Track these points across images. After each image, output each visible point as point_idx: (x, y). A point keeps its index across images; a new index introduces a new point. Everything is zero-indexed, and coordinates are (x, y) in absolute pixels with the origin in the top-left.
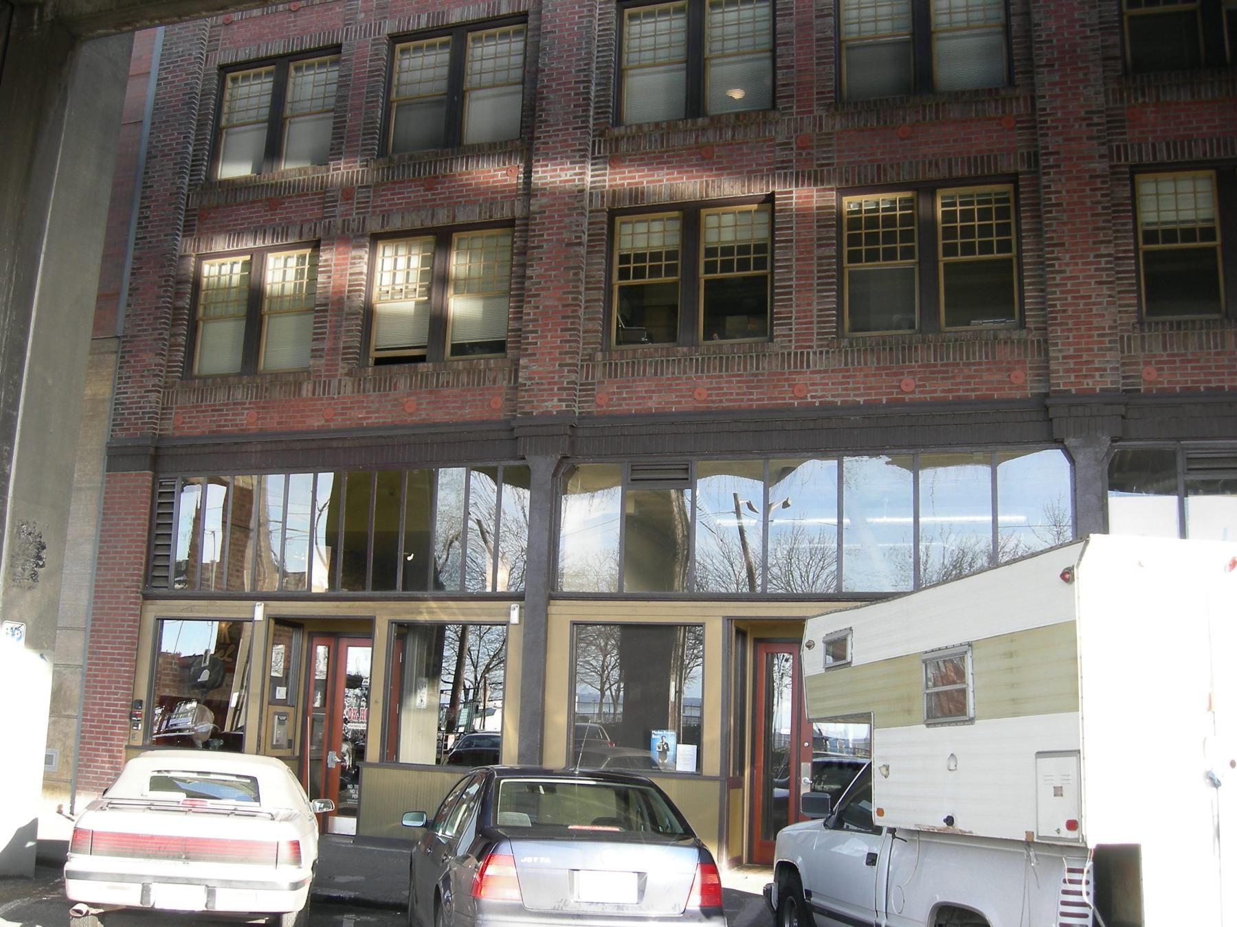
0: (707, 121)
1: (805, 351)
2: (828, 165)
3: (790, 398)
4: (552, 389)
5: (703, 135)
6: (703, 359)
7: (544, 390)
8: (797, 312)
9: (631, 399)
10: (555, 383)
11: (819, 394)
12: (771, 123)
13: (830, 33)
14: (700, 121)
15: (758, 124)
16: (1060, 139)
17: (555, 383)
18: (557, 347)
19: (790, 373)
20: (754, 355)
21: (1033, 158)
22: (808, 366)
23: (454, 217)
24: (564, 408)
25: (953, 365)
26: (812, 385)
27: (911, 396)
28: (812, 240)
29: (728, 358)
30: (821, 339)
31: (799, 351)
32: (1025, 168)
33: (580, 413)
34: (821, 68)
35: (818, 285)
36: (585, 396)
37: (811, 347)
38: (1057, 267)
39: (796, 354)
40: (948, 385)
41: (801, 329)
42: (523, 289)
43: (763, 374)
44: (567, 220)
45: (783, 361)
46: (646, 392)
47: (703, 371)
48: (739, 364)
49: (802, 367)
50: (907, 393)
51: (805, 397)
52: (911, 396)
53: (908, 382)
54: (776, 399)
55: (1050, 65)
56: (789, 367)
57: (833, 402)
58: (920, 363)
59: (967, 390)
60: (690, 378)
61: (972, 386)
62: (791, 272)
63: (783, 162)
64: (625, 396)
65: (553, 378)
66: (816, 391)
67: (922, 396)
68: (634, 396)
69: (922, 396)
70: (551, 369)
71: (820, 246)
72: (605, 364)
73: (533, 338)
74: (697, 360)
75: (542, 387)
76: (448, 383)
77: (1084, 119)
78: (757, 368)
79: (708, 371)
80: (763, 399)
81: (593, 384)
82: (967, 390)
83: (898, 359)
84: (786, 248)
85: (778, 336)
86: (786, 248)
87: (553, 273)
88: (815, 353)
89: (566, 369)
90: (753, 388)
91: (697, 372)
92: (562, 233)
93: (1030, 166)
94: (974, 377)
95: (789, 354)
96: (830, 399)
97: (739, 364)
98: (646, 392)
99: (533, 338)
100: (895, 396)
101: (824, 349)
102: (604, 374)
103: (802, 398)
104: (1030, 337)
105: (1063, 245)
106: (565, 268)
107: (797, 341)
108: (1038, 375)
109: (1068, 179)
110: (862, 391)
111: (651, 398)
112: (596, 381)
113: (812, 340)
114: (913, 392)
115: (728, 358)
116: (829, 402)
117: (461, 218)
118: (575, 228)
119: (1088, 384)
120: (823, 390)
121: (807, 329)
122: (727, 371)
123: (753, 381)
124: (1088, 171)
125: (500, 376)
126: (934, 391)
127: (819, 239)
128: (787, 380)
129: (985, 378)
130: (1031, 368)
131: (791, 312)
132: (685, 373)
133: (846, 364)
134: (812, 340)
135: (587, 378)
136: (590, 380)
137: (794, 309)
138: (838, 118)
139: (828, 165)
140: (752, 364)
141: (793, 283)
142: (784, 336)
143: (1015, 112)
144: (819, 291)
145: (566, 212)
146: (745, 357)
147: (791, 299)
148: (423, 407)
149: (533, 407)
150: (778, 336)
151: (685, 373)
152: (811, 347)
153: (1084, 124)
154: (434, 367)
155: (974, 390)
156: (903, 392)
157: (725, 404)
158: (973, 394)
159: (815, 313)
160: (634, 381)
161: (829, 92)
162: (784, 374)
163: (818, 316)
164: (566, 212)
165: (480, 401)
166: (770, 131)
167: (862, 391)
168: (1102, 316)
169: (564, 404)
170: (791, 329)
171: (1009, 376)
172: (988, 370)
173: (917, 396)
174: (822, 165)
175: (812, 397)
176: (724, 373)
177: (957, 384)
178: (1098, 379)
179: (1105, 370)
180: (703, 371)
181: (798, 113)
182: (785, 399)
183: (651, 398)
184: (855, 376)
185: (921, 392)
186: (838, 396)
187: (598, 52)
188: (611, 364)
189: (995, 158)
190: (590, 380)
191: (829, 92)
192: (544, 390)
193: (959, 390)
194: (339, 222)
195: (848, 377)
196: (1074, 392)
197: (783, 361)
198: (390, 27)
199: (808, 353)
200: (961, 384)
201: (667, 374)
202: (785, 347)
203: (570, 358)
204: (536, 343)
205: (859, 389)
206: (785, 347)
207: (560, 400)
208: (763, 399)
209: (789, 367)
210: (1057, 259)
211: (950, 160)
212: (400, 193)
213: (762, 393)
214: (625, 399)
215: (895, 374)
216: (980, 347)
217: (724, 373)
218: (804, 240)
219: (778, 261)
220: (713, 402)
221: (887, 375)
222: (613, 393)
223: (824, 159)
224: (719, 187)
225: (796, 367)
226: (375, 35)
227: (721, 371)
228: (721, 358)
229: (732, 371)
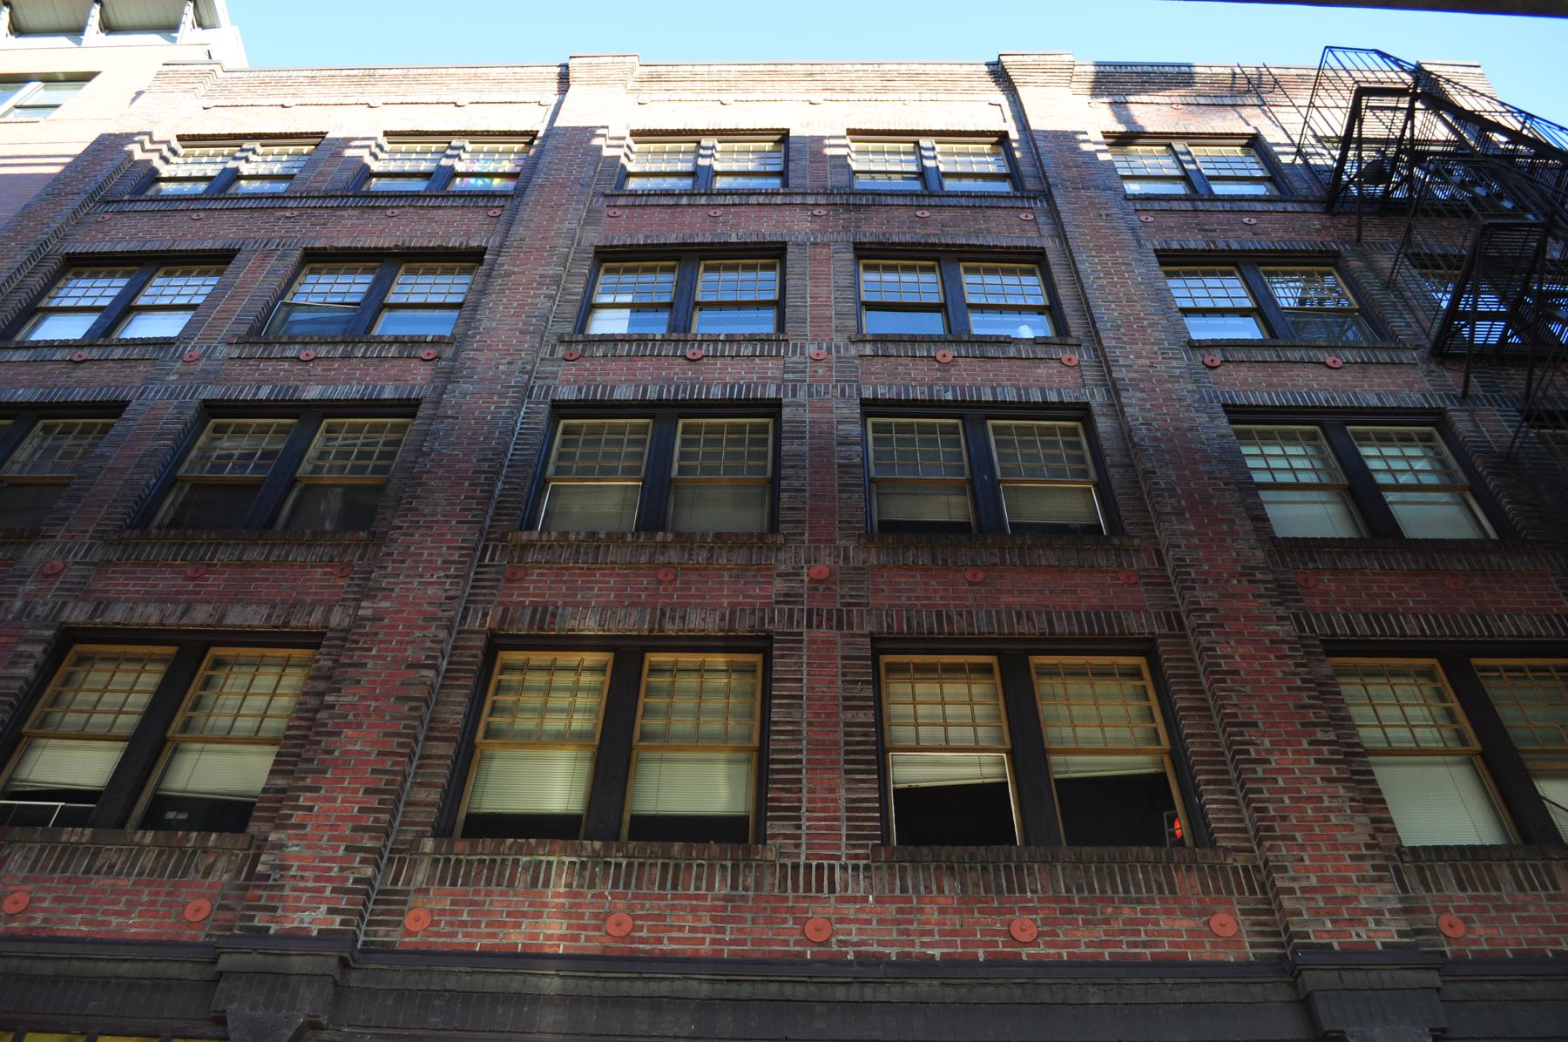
0: (670, 537)
1: (826, 863)
2: (859, 604)
3: (797, 943)
4: (320, 890)
5: (663, 554)
6: (630, 865)
7: (306, 890)
8: (810, 801)
9: (477, 924)
10: (330, 880)
11: (854, 938)
12: (770, 549)
13: (857, 460)
14: (660, 536)
15: (751, 549)
16: (1214, 594)
17: (330, 880)
18: (350, 818)
19: (797, 899)
20: (729, 863)
21: (1174, 621)
22: (832, 889)
23: (223, 617)
24: (337, 926)
25: (1101, 900)
26: (842, 921)
27: (1032, 951)
28: (835, 698)
29: (677, 866)
30: (854, 846)
31: (814, 863)
32: (1165, 630)
33: (365, 943)
34: (845, 496)
35: (846, 762)
36: (383, 913)
37: (838, 858)
38: (1253, 755)
39: (808, 867)
40: (1099, 933)
41: (816, 828)
42: (313, 720)
43: (743, 898)
44: (418, 634)
45: (784, 877)
46: (509, 914)
47: (627, 886)
48: (699, 878)
49: (820, 889)
50: (1026, 944)
51: (827, 943)
52: (1032, 951)
53: (1025, 925)
54: (769, 942)
55: (1179, 513)
56: (795, 888)
57: (883, 954)
58: (1040, 894)
59: (1135, 945)
60: (601, 896)
61: (1143, 937)
62: (800, 741)
63: (787, 595)
64: (465, 917)
65: (330, 869)
66: (849, 933)
67: (1052, 951)
68: (484, 920)
69: (1052, 951)
70: (330, 853)
71: (846, 708)
72: (437, 861)
73: (306, 799)
74: (618, 865)
75: (302, 884)
76: (111, 867)
77: (1242, 575)
78: (734, 887)
79: (638, 886)
80: (744, 942)
81: (407, 893)
82: (1135, 945)
83: (999, 886)
84: (790, 706)
85: (774, 836)
86: (790, 706)
87: (373, 704)
88: (844, 868)
89: (359, 856)
90: (724, 920)
91: (615, 885)
92: (406, 650)
93: (1171, 628)
94: (1144, 922)
95: (796, 867)
96: (875, 948)
97: (699, 878)
98: (509, 914)
99: (306, 799)
100: (1001, 949)
101: (862, 863)
102: (430, 879)
103: (820, 944)
104: (1230, 860)
105: (1255, 725)
106: (397, 698)
107: (809, 846)
108: (1259, 924)
109: (1239, 642)
110: (937, 937)
111: (518, 925)
112: (412, 887)
113: (838, 847)
114: (1033, 944)
115: (677, 866)
116: (874, 954)
117: (238, 617)
118: (429, 644)
119: (1359, 935)
120: (860, 931)
121: (827, 828)
122: (674, 887)
123: (725, 909)
124: (1267, 634)
125: (220, 866)
126: (1076, 944)
127: (846, 699)
128: (791, 910)
129: (1163, 926)
130: (1243, 912)
131: (800, 800)
132: (592, 885)
133: (904, 889)
134: (838, 847)
135: (395, 881)
136: (400, 886)
137: (805, 795)
138: (874, 551)
139: (859, 604)
140: (724, 880)
141: (803, 757)
142: (786, 836)
143: (1136, 566)
144: (847, 772)
145: (420, 622)
146: (711, 866)
147: (800, 781)
148: (45, 905)
149: (273, 920)
150: (774, 836)
151: (592, 885)
152: (838, 858)
153: (1244, 579)
154: (93, 836)
155: (1145, 945)
156: (1015, 942)
157: (667, 946)
158: (1147, 951)
159: (843, 804)
160: (488, 894)
161: (857, 522)
162: (786, 899)
163: (847, 753)
164: (420, 622)
165: (164, 904)
166: (767, 558)
167: (937, 937)
168: (1350, 828)
169: (338, 919)
170: (799, 827)
171: (1207, 923)
172: (1168, 912)
173: (1042, 950)
174: (850, 604)
175: (841, 943)
176: (669, 892)
177: (1113, 933)
178: (1372, 926)
179: (1380, 912)
180: (627, 886)
181: (849, 857)
182: (786, 943)
183: (518, 925)
184: (921, 910)
185: (1049, 945)
186: (892, 943)
187: (515, 449)
188: (448, 860)
189: (1118, 617)
190: (400, 886)
191: (857, 522)
192: (306, 890)
193: (1121, 942)
194: (18, 604)
195: (911, 911)
196: (1336, 946)
197: (784, 877)
198: (212, 392)
199: (832, 868)
200: (1122, 932)
201: (557, 885)
202: (788, 855)
203: (371, 838)
204: (310, 809)
205: (930, 933)
206: (788, 855)
207: (331, 911)
208: (744, 942)
209: (795, 888)
210: (1251, 743)
211: (1049, 614)
212: (142, 579)
213: (741, 931)
214: (464, 924)
215: (998, 911)
216: (1145, 872)
217: (669, 892)
218: (820, 699)
219: (776, 723)
220: (642, 941)
221: (981, 911)
222: (442, 912)
223: (851, 596)
224: (683, 618)
225: (808, 888)
226: (184, 398)
227: (662, 886)
228: (665, 866)
229: (686, 888)
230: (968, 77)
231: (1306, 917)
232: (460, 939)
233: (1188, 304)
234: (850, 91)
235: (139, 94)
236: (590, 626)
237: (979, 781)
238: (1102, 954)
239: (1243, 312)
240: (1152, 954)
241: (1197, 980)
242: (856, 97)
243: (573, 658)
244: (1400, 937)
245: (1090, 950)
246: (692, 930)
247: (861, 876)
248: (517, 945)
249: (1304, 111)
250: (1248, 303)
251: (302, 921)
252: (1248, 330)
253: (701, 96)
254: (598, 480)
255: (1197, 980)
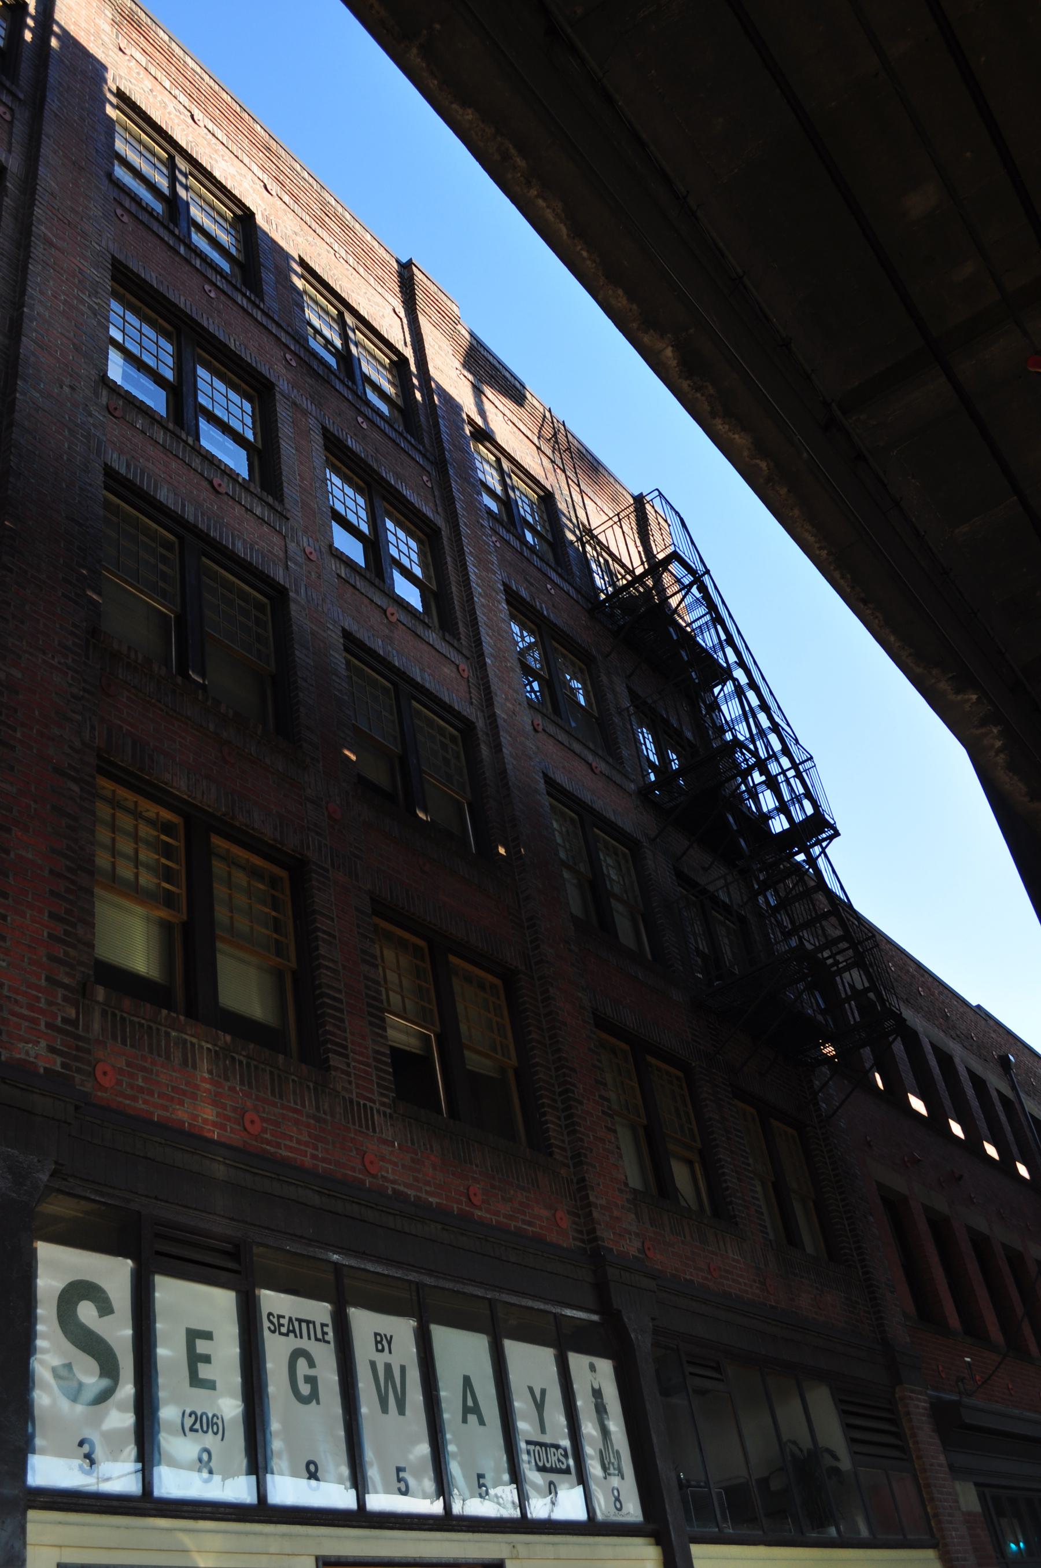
37: (374, 1102)
78: (318, 1109)
158: (530, 1229)
230: (383, 264)
231: (603, 1227)
232: (140, 1105)
233: (339, 507)
234: (296, 200)
235: (120, 49)
236: (180, 785)
237: (408, 1049)
238: (387, 1188)
239: (159, 380)
240: (515, 1227)
241: (273, 1176)
242: (296, 208)
243: (152, 810)
244: (62, 1068)
245: (505, 1220)
246: (299, 1142)
247: (389, 1124)
248: (184, 1122)
249: (618, 523)
250: (169, 375)
251: (27, 1053)
252: (155, 399)
253: (176, 92)
254: (141, 592)
255: (273, 1176)
